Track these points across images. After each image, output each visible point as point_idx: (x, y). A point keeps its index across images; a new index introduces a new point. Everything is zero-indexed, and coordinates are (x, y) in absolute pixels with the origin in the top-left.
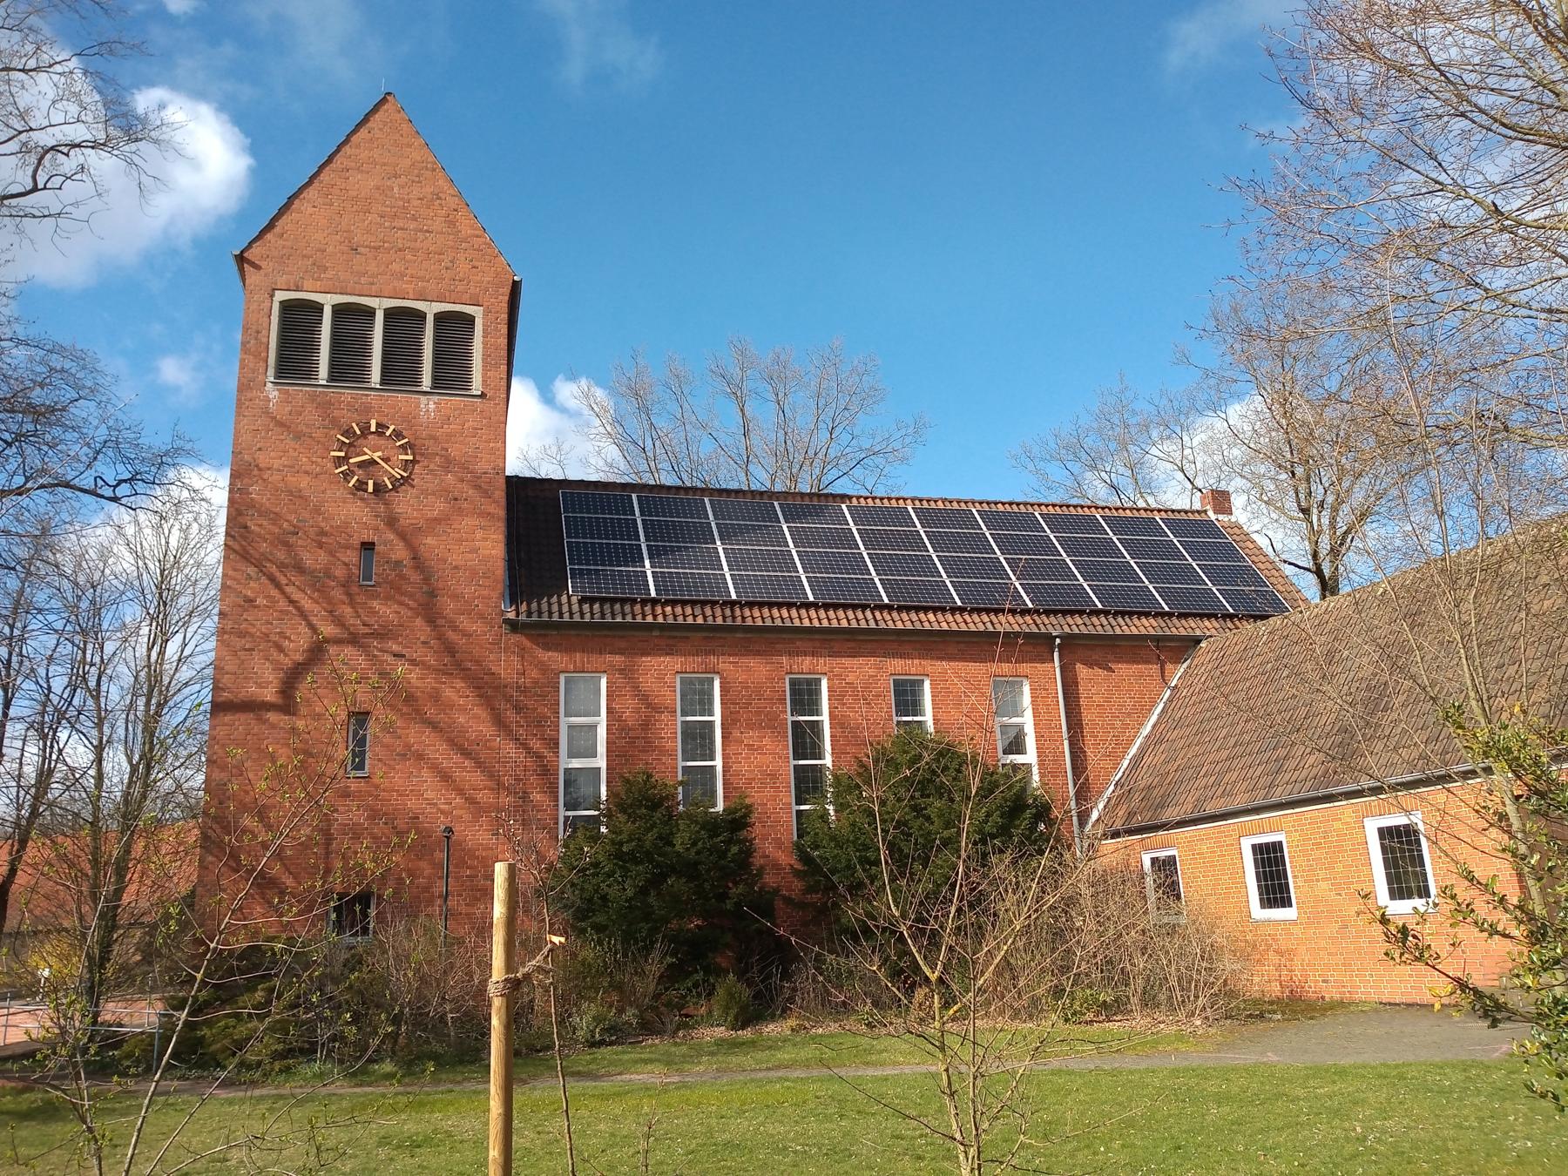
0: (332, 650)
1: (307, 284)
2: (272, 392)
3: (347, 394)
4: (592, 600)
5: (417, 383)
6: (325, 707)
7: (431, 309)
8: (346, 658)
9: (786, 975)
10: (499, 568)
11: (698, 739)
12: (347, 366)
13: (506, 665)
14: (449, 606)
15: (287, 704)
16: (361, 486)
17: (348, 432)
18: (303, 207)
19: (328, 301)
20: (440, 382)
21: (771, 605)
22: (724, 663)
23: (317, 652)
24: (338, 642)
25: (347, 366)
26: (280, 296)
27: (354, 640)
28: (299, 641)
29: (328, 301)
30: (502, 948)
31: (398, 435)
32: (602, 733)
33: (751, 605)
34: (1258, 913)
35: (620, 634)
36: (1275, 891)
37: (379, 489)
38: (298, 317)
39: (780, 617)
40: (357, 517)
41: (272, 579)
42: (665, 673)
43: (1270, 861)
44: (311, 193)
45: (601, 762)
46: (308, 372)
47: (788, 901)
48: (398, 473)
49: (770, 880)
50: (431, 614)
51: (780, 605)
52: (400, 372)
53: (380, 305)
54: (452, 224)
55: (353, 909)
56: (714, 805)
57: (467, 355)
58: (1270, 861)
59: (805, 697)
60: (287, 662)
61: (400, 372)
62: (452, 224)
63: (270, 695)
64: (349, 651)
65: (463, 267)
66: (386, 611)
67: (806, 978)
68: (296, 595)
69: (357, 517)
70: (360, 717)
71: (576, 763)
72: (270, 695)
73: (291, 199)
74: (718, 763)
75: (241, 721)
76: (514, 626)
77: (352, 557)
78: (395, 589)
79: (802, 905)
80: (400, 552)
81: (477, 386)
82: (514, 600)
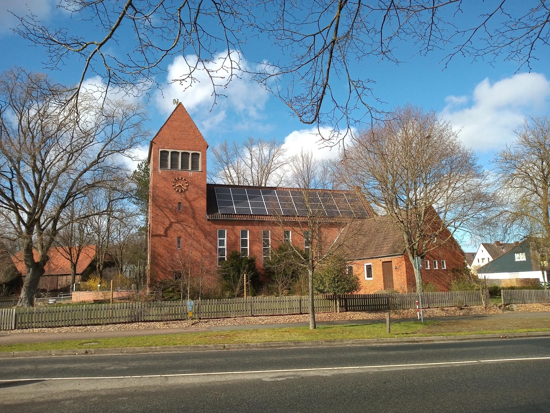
0: (174, 224)
1: (165, 147)
2: (160, 171)
3: (174, 171)
4: (223, 214)
5: (188, 168)
6: (173, 236)
7: (191, 152)
8: (177, 226)
9: (262, 288)
10: (206, 209)
11: (244, 243)
12: (174, 165)
13: (208, 228)
14: (197, 216)
15: (166, 235)
16: (178, 191)
17: (175, 179)
18: (164, 130)
19: (170, 151)
20: (193, 168)
21: (259, 215)
22: (250, 227)
23: (171, 224)
24: (175, 223)
25: (174, 165)
26: (160, 150)
27: (178, 222)
28: (167, 223)
29: (170, 151)
30: (209, 282)
31: (185, 180)
32: (225, 241)
33: (255, 215)
34: (366, 278)
35: (230, 221)
36: (369, 275)
37: (182, 191)
38: (164, 154)
39: (261, 218)
40: (177, 197)
41: (161, 210)
42: (239, 229)
43: (369, 268)
44: (165, 127)
45: (225, 247)
46: (166, 166)
47: (262, 275)
48: (185, 188)
49: (258, 271)
50: (194, 218)
51: (261, 215)
52: (185, 166)
53: (180, 151)
54: (194, 133)
55: (385, 383)
56: (427, 267)
57: (198, 162)
58: (369, 268)
59: (265, 234)
60: (165, 227)
61: (185, 166)
62: (194, 133)
63: (162, 233)
64: (177, 225)
65: (197, 143)
66: (182, 216)
67: (265, 288)
68: (166, 213)
69: (177, 197)
70: (179, 238)
71: (221, 247)
72: (162, 233)
73: (161, 128)
74: (248, 247)
75: (157, 238)
76: (209, 220)
77: (176, 205)
78: (185, 211)
79: (264, 276)
80: (187, 204)
81: (200, 169)
82: (208, 214)
